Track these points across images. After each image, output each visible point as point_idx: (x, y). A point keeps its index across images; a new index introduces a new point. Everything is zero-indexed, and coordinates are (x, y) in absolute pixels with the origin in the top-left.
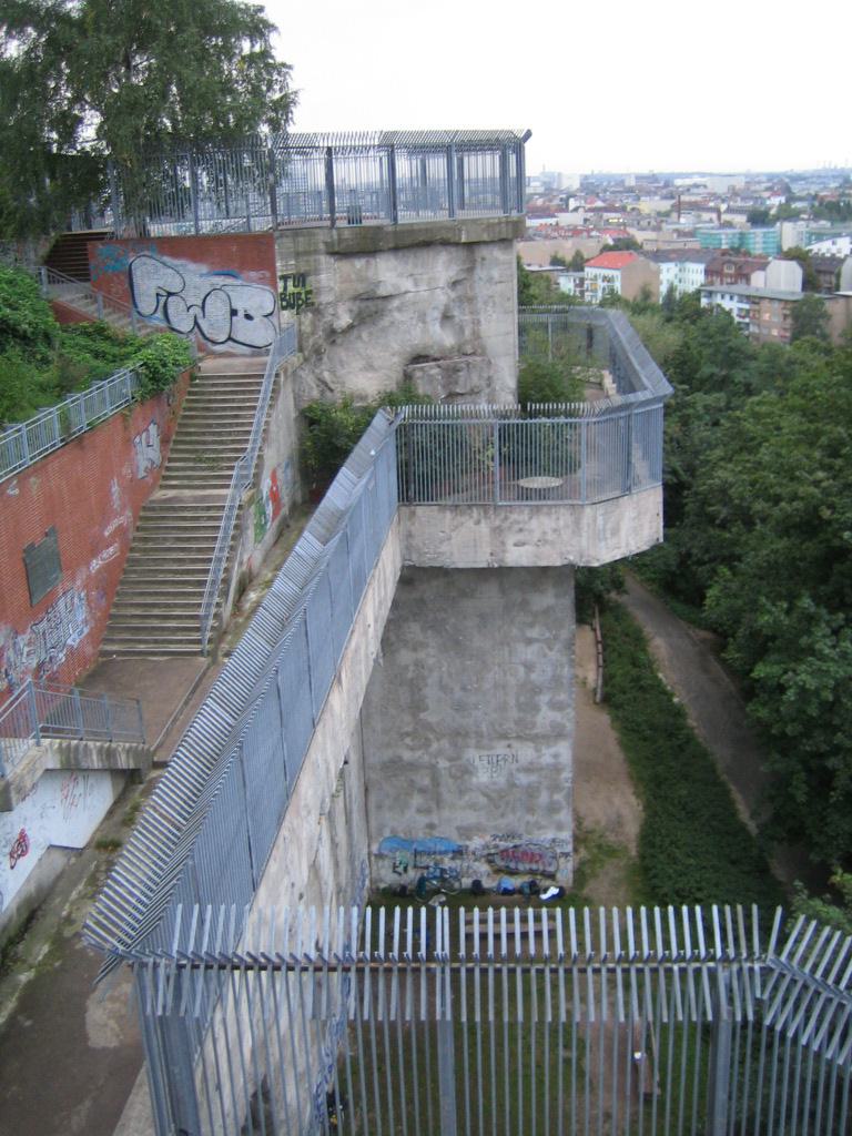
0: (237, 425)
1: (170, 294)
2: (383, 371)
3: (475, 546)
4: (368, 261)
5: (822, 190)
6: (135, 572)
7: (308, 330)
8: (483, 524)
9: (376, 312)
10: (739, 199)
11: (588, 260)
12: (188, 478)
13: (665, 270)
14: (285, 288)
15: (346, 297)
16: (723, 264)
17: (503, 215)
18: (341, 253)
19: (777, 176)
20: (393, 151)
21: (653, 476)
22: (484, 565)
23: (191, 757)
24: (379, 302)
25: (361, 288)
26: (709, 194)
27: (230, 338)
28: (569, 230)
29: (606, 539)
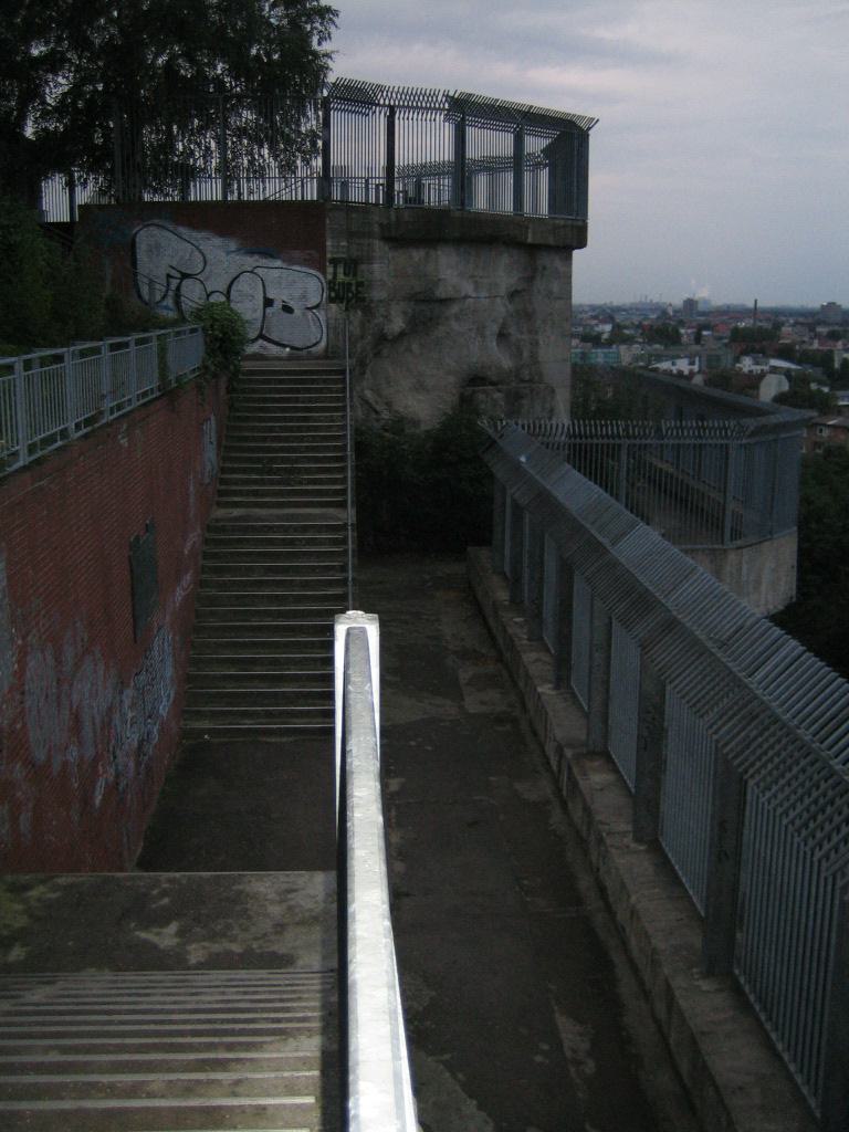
0: (309, 429)
1: (185, 276)
4: (427, 253)
5: (644, 319)
6: (212, 614)
7: (357, 332)
9: (431, 319)
12: (256, 493)
14: (335, 274)
18: (399, 238)
19: (600, 307)
23: (795, 930)
27: (261, 336)
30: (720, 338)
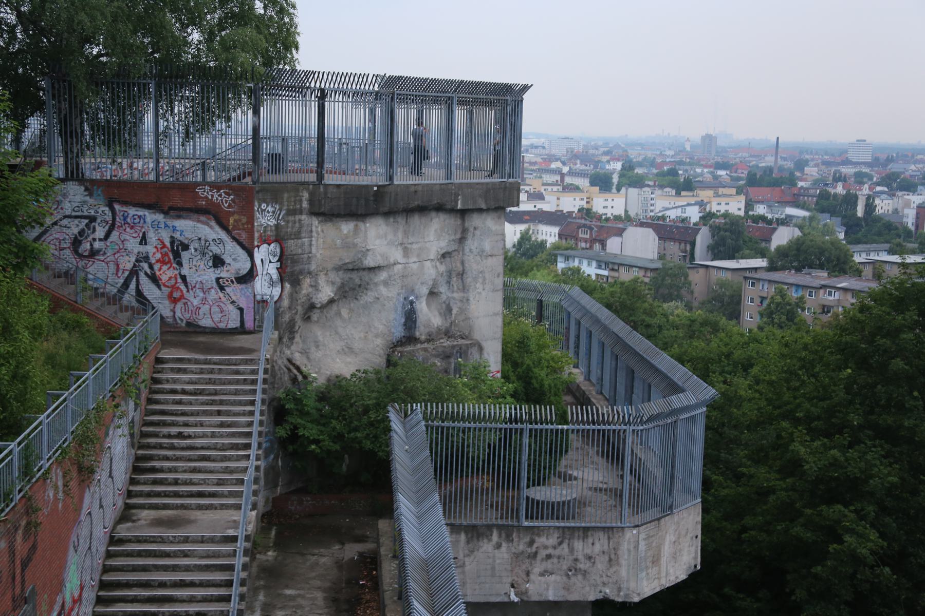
9: (360, 286)
10: (578, 162)
15: (330, 266)
16: (579, 228)
24: (365, 273)
25: (347, 257)
30: (739, 179)
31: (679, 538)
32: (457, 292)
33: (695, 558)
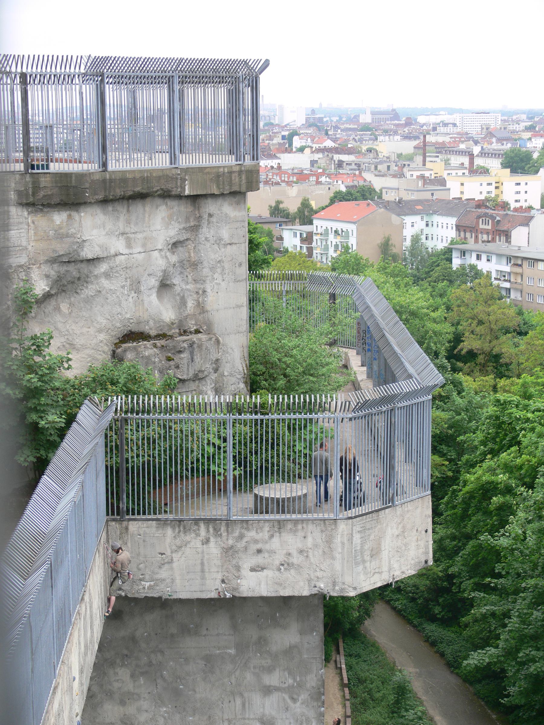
2: (88, 351)
3: (203, 571)
4: (70, 216)
8: (212, 544)
9: (79, 279)
10: (494, 140)
11: (316, 212)
13: (409, 225)
15: (42, 258)
16: (479, 217)
17: (234, 162)
20: (102, 81)
21: (418, 483)
22: (213, 595)
24: (83, 265)
25: (61, 248)
26: (458, 133)
28: (294, 174)
29: (364, 561)
31: (403, 532)
32: (191, 283)
33: (427, 553)
